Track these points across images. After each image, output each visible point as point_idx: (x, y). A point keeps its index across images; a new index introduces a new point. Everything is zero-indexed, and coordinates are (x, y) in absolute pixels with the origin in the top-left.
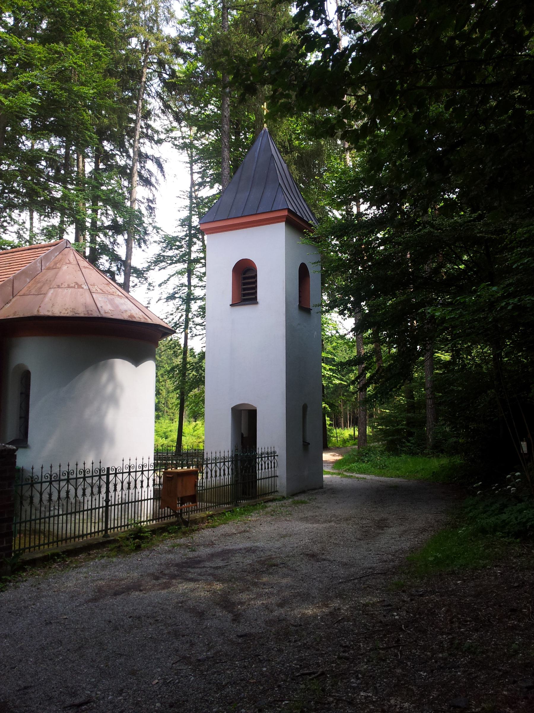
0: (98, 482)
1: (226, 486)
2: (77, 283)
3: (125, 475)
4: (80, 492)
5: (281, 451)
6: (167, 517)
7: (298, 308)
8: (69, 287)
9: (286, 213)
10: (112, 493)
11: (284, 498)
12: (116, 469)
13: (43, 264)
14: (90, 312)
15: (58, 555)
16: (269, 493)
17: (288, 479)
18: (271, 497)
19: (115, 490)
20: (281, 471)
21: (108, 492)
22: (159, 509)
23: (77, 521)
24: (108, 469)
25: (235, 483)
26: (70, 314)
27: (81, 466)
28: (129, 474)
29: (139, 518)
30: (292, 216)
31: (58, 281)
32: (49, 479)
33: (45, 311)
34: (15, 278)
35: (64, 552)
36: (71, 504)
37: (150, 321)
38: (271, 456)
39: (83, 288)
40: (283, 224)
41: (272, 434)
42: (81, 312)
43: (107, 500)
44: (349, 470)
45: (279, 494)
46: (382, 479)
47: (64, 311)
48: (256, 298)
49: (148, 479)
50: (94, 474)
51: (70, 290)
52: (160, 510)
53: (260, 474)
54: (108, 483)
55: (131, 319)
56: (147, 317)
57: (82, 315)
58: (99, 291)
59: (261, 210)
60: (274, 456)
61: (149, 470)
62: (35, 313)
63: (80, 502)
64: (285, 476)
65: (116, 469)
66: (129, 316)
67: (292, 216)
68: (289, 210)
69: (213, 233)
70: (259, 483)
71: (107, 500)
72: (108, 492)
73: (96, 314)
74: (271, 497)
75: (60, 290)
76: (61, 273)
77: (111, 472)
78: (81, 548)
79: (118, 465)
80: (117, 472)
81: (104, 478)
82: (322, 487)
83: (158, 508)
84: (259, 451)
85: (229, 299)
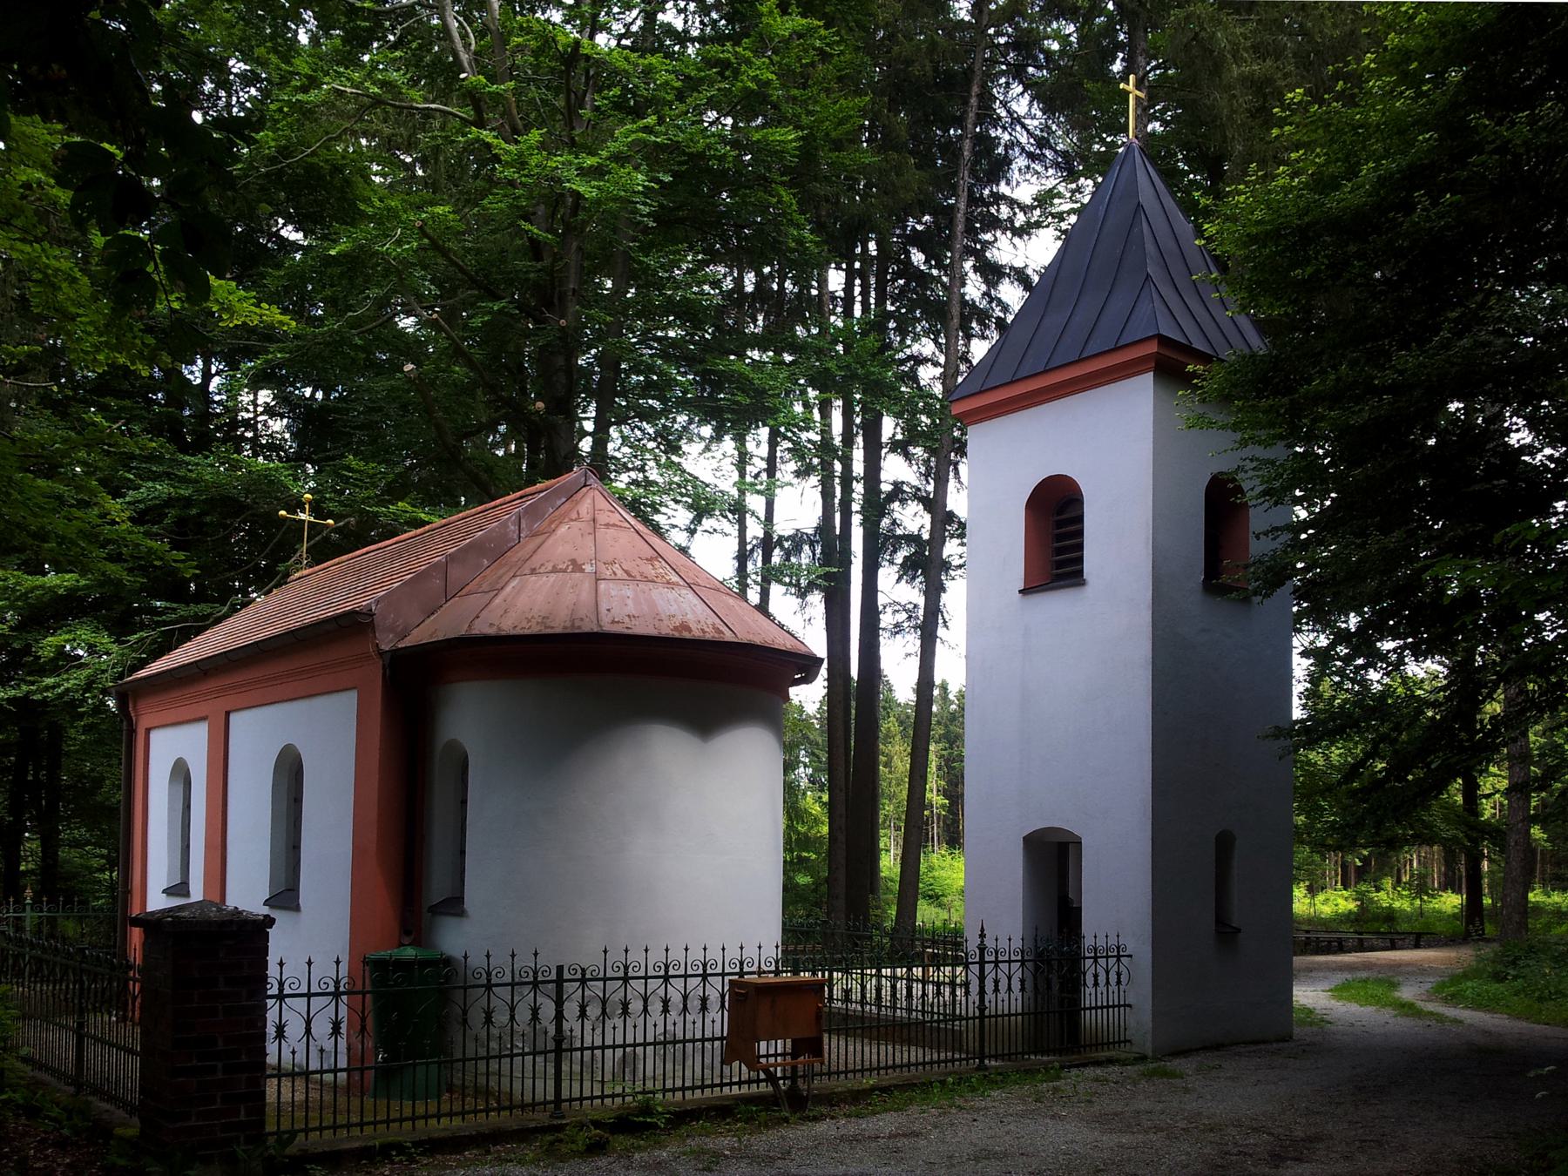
0: (516, 999)
1: (1003, 1016)
2: (574, 562)
3: (1112, 961)
4: (572, 1009)
5: (1139, 945)
6: (871, 1070)
7: (1200, 587)
8: (555, 570)
9: (1153, 348)
10: (990, 995)
11: (1143, 1058)
12: (583, 970)
13: (523, 525)
14: (577, 623)
15: (400, 1148)
16: (1108, 1043)
17: (1156, 1014)
18: (1104, 1054)
19: (996, 990)
20: (1140, 992)
21: (982, 992)
22: (722, 1063)
23: (518, 1074)
24: (560, 969)
25: (1035, 1015)
26: (535, 629)
27: (616, 957)
28: (996, 966)
29: (639, 1083)
30: (1168, 353)
31: (535, 561)
32: (662, 973)
33: (482, 628)
34: (451, 558)
35: (416, 1144)
36: (322, 1050)
37: (728, 636)
38: (1107, 957)
39: (582, 571)
40: (1149, 377)
41: (1117, 900)
42: (558, 626)
43: (982, 1007)
44: (1453, 996)
45: (1135, 1049)
46: (1539, 1028)
47: (524, 624)
48: (1081, 571)
49: (1010, 978)
50: (690, 972)
51: (553, 577)
52: (726, 1069)
53: (1089, 996)
54: (982, 978)
55: (677, 635)
56: (724, 629)
57: (559, 630)
58: (620, 573)
59: (1093, 348)
60: (1118, 957)
61: (1010, 962)
62: (462, 631)
63: (322, 1050)
64: (1148, 1006)
65: (583, 970)
66: (676, 628)
67: (1168, 353)
68: (1163, 340)
69: (981, 421)
70: (1088, 1017)
71: (982, 1007)
72: (982, 992)
73: (588, 627)
74: (1104, 1054)
75: (534, 578)
76: (550, 541)
77: (566, 976)
78: (470, 1137)
79: (589, 958)
80: (287, 991)
81: (975, 968)
82: (1287, 1038)
83: (718, 1060)
84: (1088, 942)
85: (1017, 578)
